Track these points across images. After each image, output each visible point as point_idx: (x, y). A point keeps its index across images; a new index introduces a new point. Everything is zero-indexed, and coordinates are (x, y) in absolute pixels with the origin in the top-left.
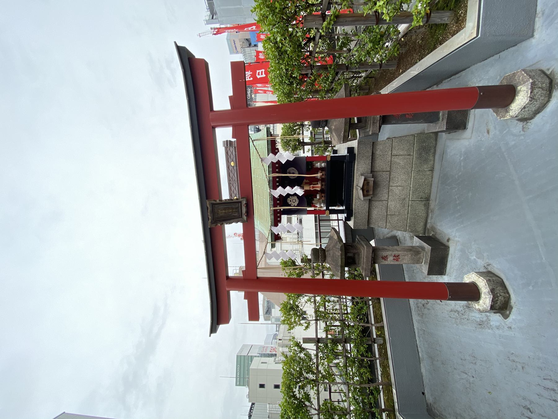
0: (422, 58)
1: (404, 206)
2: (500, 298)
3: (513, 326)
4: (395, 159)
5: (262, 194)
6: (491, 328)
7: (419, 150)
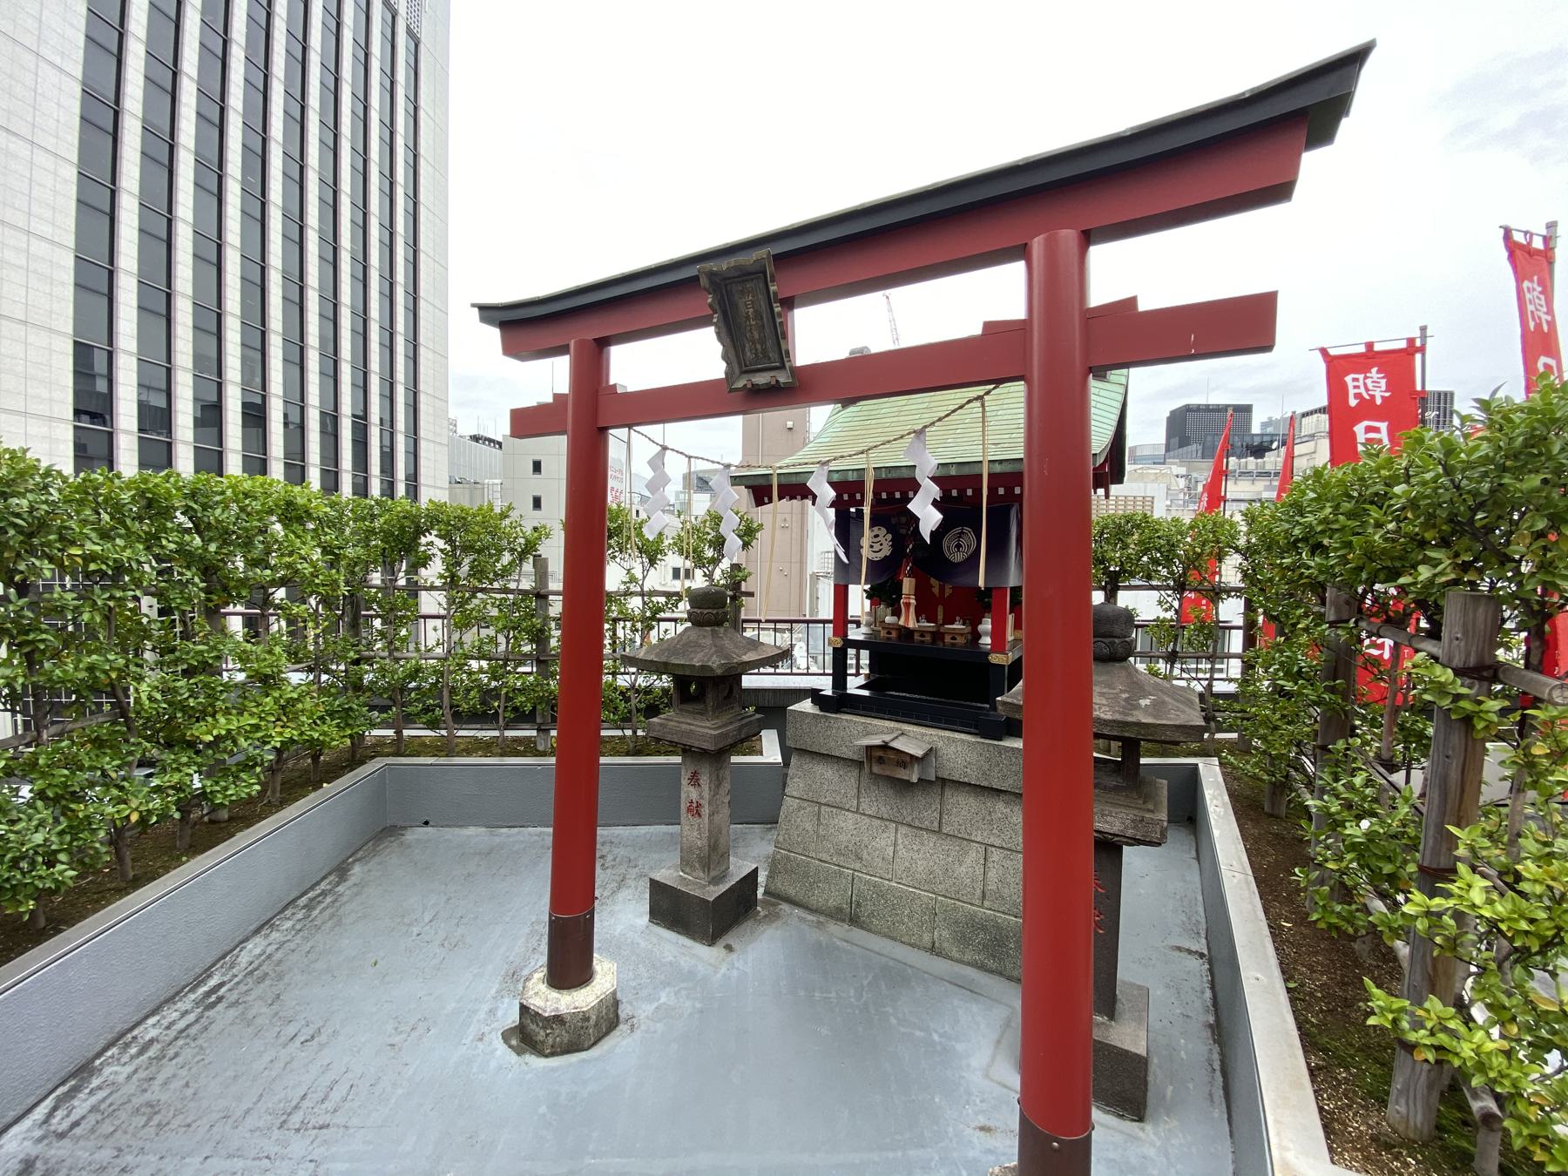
0: (1292, 1001)
1: (839, 853)
2: (542, 1033)
3: (481, 1045)
4: (974, 855)
5: (824, 435)
6: (499, 995)
7: (997, 927)
